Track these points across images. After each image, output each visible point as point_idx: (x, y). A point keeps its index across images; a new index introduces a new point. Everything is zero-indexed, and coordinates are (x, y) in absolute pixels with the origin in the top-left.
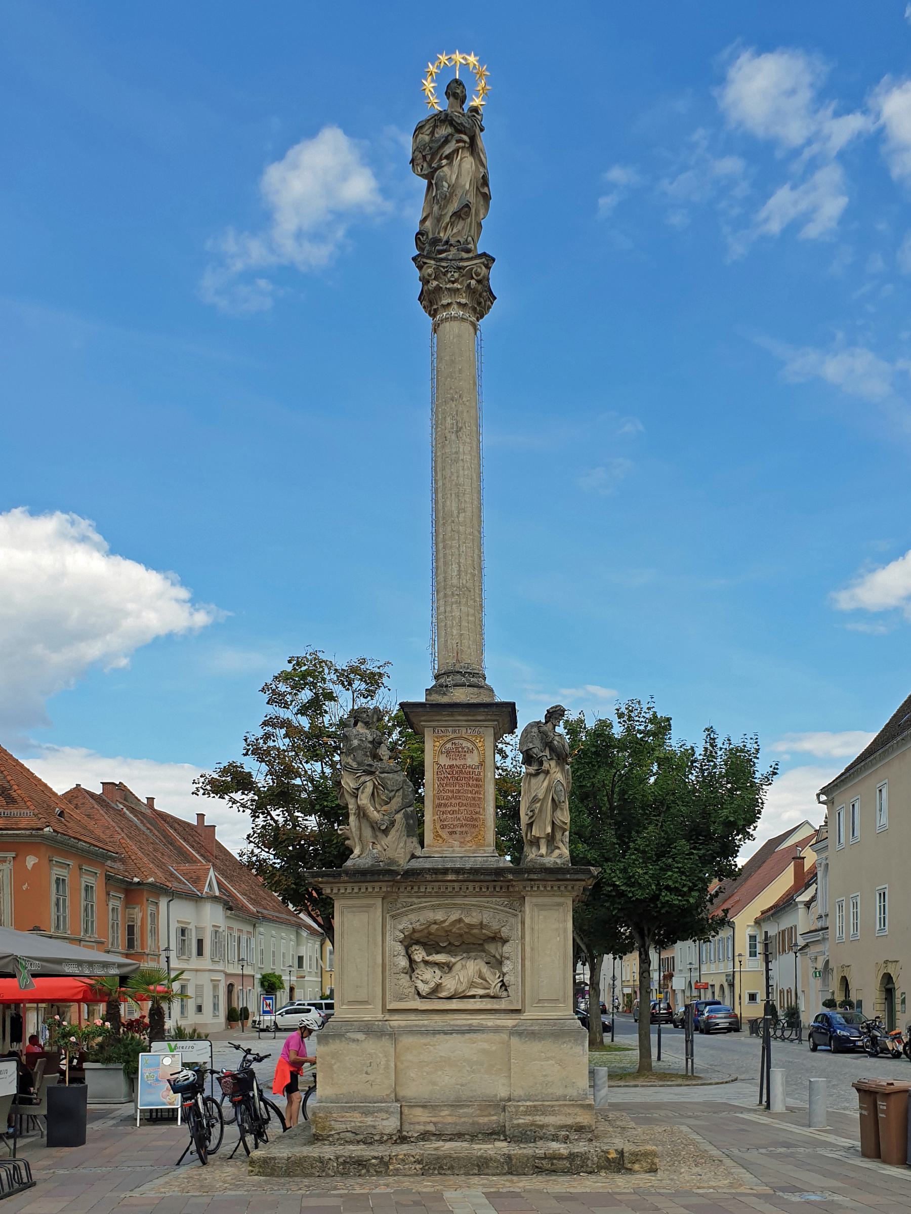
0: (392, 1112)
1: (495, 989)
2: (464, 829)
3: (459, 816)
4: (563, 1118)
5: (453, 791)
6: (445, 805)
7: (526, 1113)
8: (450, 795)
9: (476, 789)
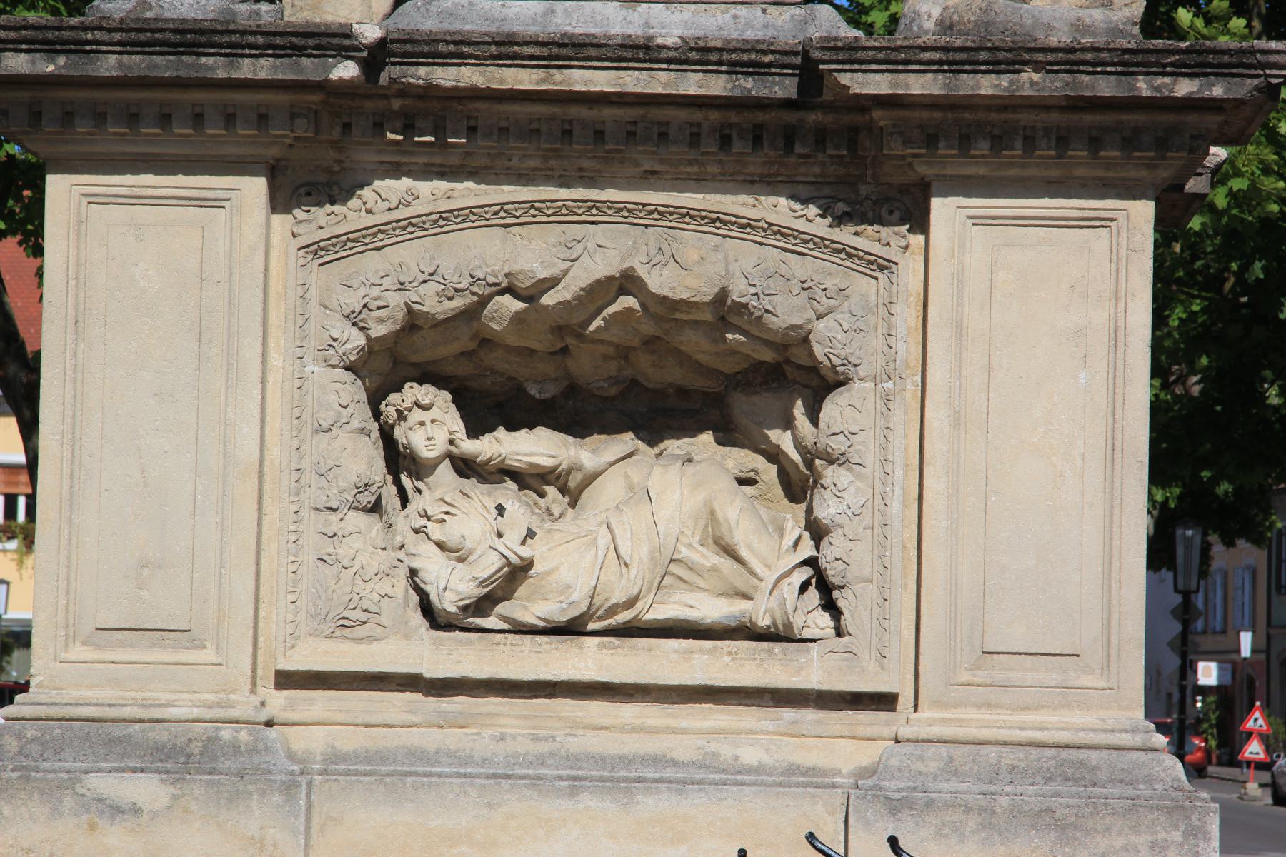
1: (778, 596)
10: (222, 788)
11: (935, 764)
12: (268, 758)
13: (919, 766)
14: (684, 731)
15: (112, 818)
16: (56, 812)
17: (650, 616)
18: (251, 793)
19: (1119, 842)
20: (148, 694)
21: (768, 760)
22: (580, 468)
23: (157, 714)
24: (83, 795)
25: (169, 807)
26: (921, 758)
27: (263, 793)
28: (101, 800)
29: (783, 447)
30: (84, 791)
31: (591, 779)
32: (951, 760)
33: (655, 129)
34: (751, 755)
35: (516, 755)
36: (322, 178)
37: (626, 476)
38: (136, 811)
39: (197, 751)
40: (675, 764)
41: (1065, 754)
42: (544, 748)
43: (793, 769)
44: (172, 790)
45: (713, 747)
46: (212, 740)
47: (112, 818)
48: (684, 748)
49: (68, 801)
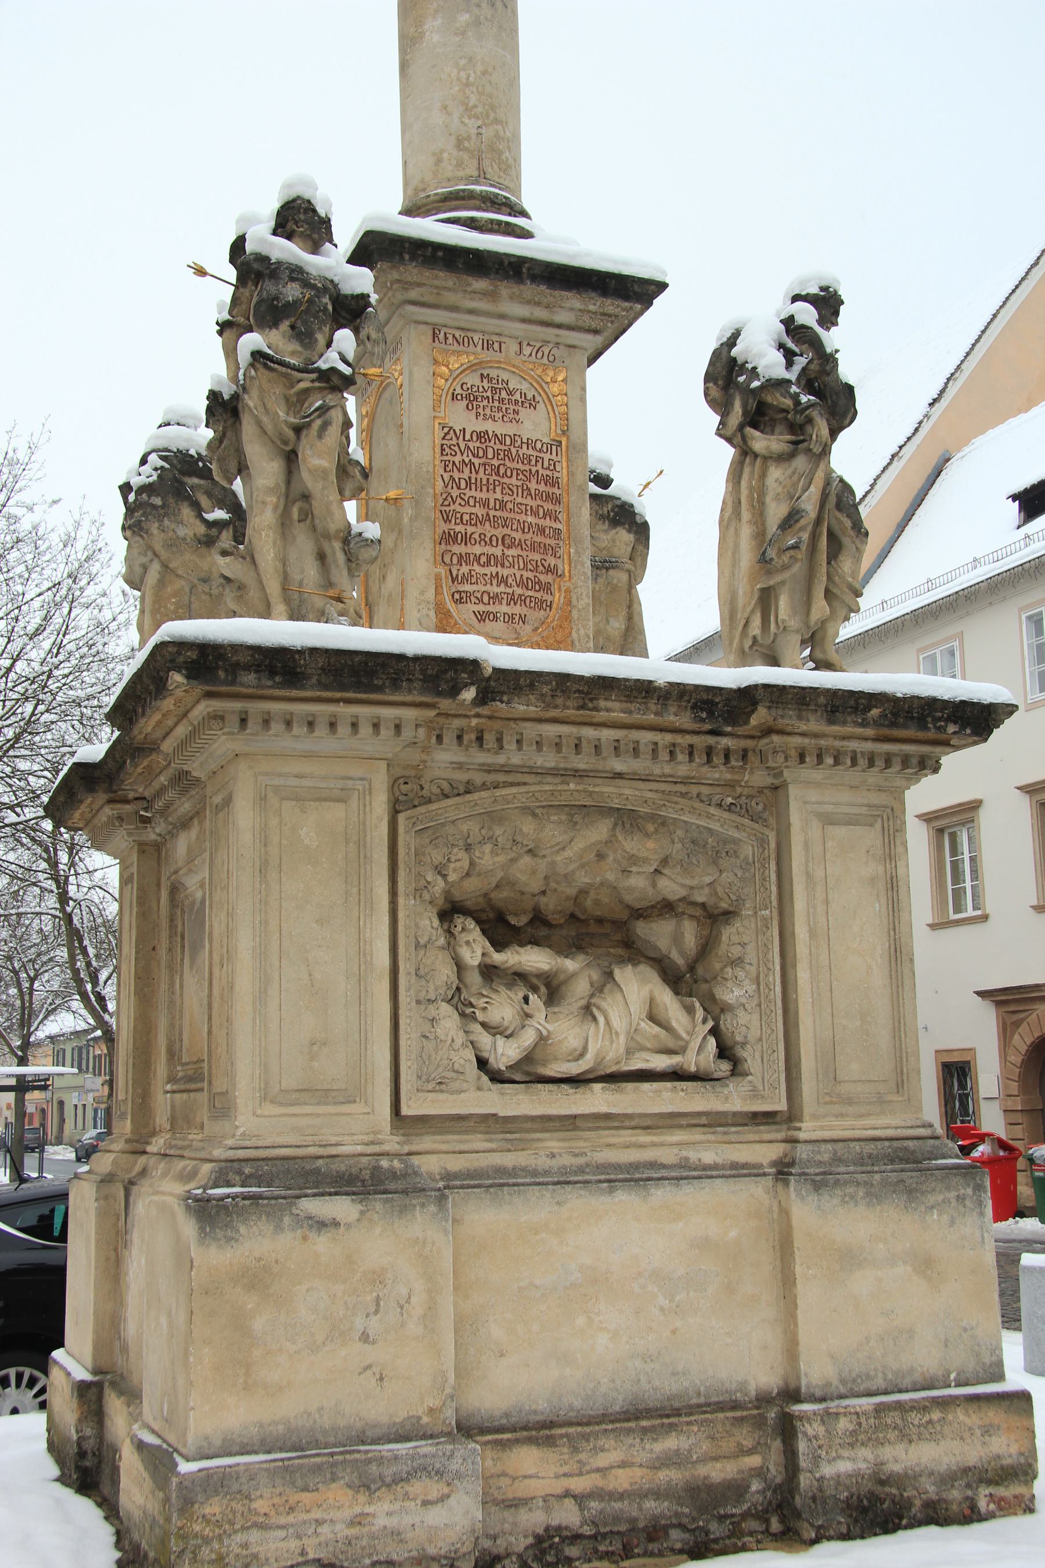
0: (459, 1476)
1: (700, 1054)
2: (517, 609)
3: (505, 572)
4: (955, 1446)
5: (485, 504)
6: (466, 539)
7: (853, 1440)
8: (480, 511)
9: (548, 506)
10: (395, 1204)
11: (827, 1156)
12: (418, 1179)
13: (818, 1157)
14: (662, 1145)
15: (319, 1231)
16: (279, 1229)
17: (626, 1068)
18: (415, 1206)
19: (940, 1198)
20: (321, 1137)
21: (719, 1161)
22: (565, 971)
23: (333, 1151)
24: (298, 1215)
25: (358, 1220)
26: (819, 1152)
27: (423, 1205)
28: (310, 1218)
29: (671, 956)
30: (298, 1212)
31: (620, 1181)
32: (835, 1153)
33: (631, 746)
34: (708, 1157)
35: (565, 1167)
36: (412, 773)
37: (590, 976)
38: (336, 1224)
39: (367, 1177)
40: (664, 1166)
41: (895, 1144)
42: (581, 1161)
43: (734, 1166)
44: (360, 1207)
45: (684, 1153)
46: (377, 1168)
47: (319, 1231)
48: (667, 1156)
49: (287, 1220)
